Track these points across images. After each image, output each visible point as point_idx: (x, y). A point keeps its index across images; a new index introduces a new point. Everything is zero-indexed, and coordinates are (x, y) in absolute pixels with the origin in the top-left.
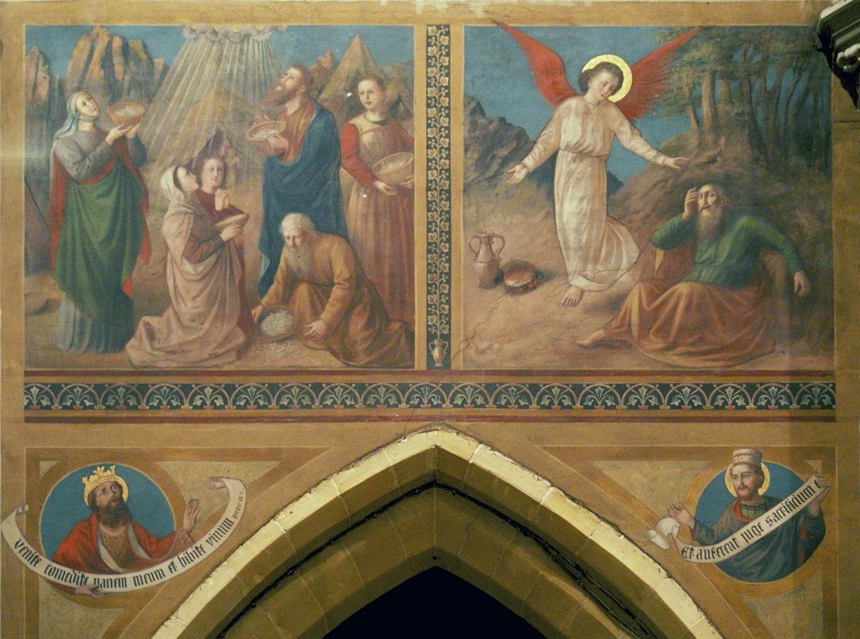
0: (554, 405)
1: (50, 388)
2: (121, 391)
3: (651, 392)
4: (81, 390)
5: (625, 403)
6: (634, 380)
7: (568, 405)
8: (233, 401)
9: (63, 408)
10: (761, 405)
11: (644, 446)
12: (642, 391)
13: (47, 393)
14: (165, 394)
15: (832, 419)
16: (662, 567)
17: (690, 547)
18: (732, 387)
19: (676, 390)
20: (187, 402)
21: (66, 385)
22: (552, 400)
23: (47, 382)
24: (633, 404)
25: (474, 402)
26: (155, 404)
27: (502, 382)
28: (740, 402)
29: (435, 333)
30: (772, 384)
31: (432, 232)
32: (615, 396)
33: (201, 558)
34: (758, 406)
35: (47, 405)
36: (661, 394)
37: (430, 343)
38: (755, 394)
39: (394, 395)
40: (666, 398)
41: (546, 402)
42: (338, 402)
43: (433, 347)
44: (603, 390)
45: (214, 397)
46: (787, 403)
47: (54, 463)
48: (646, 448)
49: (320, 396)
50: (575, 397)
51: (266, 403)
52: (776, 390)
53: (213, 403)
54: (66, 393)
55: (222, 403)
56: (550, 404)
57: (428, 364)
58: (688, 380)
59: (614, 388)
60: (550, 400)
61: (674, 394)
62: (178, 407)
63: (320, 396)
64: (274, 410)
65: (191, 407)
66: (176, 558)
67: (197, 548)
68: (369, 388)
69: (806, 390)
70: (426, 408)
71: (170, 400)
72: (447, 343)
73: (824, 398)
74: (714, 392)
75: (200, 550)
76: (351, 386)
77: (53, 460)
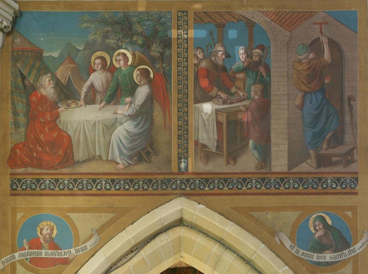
0: (178, 188)
1: (204, 181)
2: (291, 181)
3: (333, 181)
4: (255, 181)
5: (40, 188)
6: (212, 176)
7: (109, 188)
8: (265, 186)
9: (342, 189)
10: (230, 188)
11: (279, 205)
12: (254, 181)
13: (53, 183)
14: (235, 183)
15: (356, 194)
16: (125, 257)
17: (294, 246)
18: (30, 180)
19: (287, 181)
20: (245, 186)
21: (230, 179)
22: (158, 186)
23: (278, 177)
24: (25, 188)
25: (256, 187)
26: (268, 187)
27: (136, 178)
28: (296, 186)
29: (181, 156)
30: (103, 179)
31: (180, 112)
32: (166, 184)
33: (7, 257)
34: (247, 188)
35: (297, 187)
36: (318, 183)
37: (179, 161)
38: (115, 184)
39: (203, 184)
40: (283, 184)
41: (117, 187)
42: (47, 187)
43: (181, 162)
44: (49, 181)
45: (332, 183)
46: (241, 187)
47: (251, 213)
48: (279, 206)
49: (77, 185)
50: (56, 185)
51: (279, 187)
52: (236, 181)
53: (124, 188)
54: (343, 182)
55: (260, 187)
56: (251, 187)
57: (178, 170)
58: (67, 177)
59: (129, 181)
60: (138, 187)
61: (305, 182)
62: (241, 189)
63: (77, 185)
64: (169, 190)
65: (284, 188)
66: (317, 254)
67: (350, 250)
68: (61, 181)
69: (287, 181)
70: (348, 189)
71: (237, 185)
72: (186, 161)
73: (70, 185)
74: (247, 181)
75: (354, 251)
76: (146, 180)
77: (251, 215)
